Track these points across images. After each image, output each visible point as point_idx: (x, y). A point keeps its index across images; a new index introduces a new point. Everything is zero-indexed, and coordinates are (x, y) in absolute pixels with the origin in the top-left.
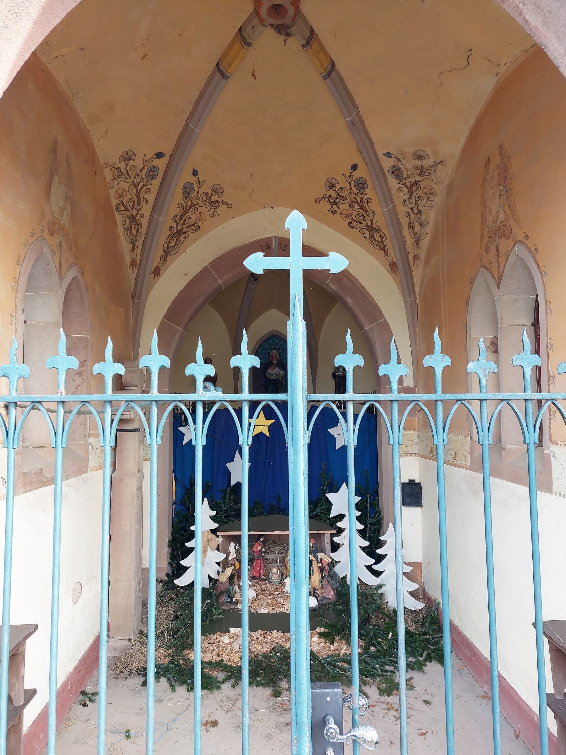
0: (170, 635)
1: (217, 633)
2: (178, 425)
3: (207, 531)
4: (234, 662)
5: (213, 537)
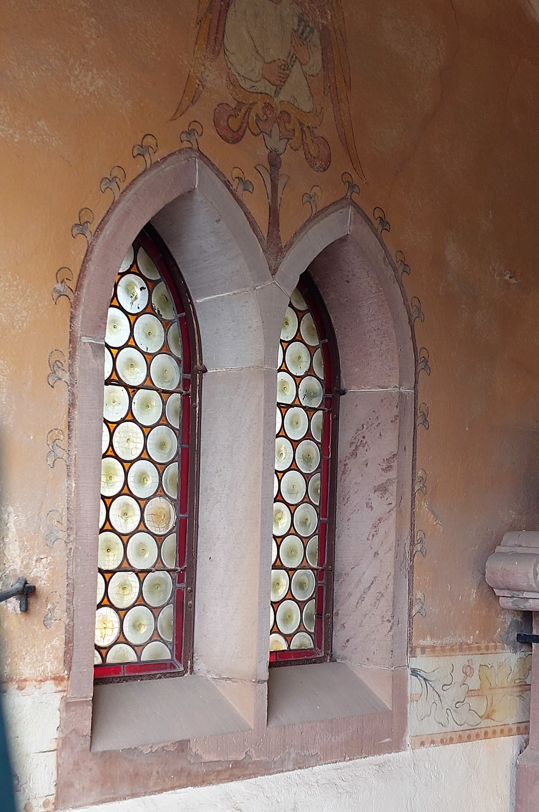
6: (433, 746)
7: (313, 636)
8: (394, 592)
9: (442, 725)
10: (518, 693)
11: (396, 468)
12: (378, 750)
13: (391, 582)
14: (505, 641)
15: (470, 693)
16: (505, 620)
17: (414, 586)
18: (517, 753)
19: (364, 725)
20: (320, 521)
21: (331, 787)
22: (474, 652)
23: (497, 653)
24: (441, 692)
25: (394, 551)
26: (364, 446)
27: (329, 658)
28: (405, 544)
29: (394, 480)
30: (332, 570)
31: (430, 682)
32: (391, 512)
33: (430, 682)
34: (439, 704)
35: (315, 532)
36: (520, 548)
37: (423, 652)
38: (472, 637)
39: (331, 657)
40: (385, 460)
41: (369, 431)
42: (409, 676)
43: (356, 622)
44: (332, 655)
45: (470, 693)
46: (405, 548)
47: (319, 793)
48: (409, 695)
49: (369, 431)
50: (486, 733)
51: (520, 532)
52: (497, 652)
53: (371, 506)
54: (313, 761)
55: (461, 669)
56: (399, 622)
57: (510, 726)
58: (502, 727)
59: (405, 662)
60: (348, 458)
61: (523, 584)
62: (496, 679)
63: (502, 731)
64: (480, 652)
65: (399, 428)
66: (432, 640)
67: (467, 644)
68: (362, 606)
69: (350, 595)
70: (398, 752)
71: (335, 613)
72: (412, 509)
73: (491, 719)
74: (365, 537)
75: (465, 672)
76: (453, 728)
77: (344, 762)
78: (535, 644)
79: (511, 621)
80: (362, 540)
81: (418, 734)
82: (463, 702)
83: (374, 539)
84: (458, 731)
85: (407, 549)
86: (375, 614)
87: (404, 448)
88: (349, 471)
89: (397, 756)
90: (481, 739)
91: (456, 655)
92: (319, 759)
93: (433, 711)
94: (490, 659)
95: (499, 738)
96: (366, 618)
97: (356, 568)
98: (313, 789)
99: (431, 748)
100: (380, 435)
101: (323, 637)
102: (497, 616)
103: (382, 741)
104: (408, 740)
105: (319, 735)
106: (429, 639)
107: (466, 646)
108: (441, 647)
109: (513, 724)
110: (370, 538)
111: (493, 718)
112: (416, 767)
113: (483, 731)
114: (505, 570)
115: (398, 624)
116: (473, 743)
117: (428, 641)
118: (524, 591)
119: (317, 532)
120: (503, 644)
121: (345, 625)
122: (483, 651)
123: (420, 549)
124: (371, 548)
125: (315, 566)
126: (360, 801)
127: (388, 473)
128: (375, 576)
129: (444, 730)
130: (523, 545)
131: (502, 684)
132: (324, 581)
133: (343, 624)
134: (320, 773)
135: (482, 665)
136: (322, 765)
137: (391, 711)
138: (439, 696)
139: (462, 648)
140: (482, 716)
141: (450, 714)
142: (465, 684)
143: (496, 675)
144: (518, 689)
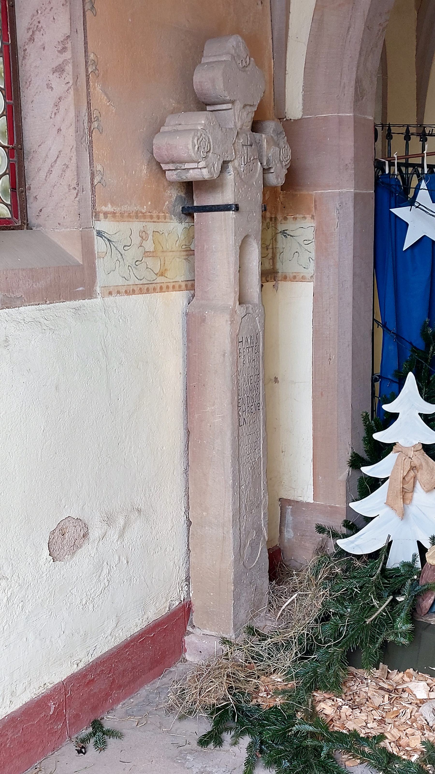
0: (303, 651)
1: (408, 671)
2: (393, 202)
3: (414, 447)
4: (407, 748)
5: (427, 463)
6: (119, 295)
7: (10, 207)
8: (77, 163)
9: (125, 279)
10: (185, 257)
11: (70, 48)
12: (73, 296)
13: (74, 154)
14: (173, 213)
15: (146, 254)
16: (172, 195)
17: (94, 159)
18: (186, 305)
19: (60, 275)
20: (7, 103)
21: (36, 324)
22: (147, 220)
23: (166, 222)
24: (123, 252)
25: (74, 126)
26: (40, 31)
27: (25, 226)
28: (84, 120)
29: (69, 61)
30: (22, 149)
31: (113, 243)
32: (69, 90)
33: (113, 243)
34: (122, 262)
35: (3, 113)
36: (180, 126)
37: (106, 217)
38: (145, 207)
39: (28, 225)
40: (60, 42)
41: (43, 16)
42: (95, 237)
43: (47, 193)
44: (28, 224)
45: (146, 254)
46: (84, 124)
47: (26, 329)
48: (96, 252)
49: (43, 16)
50: (161, 288)
51: (179, 114)
52: (166, 221)
53: (51, 87)
54: (19, 302)
55: (138, 233)
56: (83, 189)
57: (179, 283)
58: (174, 284)
59: (91, 225)
60: (26, 44)
61: (184, 155)
62: (167, 244)
63: (174, 287)
64: (152, 220)
65: (70, 11)
66: (112, 207)
67: (141, 212)
68: (50, 178)
69: (39, 170)
70: (91, 299)
71: (28, 188)
72: (88, 89)
73: (165, 276)
74: (48, 117)
75: (141, 236)
76: (135, 282)
77: (46, 305)
78: (196, 213)
79: (176, 195)
80: (46, 119)
81: (107, 286)
82: (141, 261)
83: (56, 117)
84: (139, 284)
85: (86, 125)
86: (63, 184)
87: (76, 31)
88: (28, 56)
89: (90, 302)
90: (157, 292)
91: (133, 221)
92: (24, 301)
93: (117, 267)
94: (160, 227)
95: (172, 292)
96: (55, 188)
97: (42, 146)
98: (21, 325)
99: (118, 297)
100: (54, 19)
101: (19, 208)
102: (165, 191)
103: (76, 289)
104: (98, 290)
105: (21, 281)
106: (109, 206)
107: (140, 214)
108: (121, 213)
109: (182, 281)
110: (53, 116)
111: (166, 276)
112: (107, 312)
113: (159, 286)
114: (169, 144)
115: (83, 191)
116: (151, 295)
117: (109, 208)
118: (185, 163)
119: (7, 172)
120: (171, 215)
121: (37, 197)
122: (155, 220)
123: (97, 126)
124: (54, 126)
125: (6, 145)
126: (61, 337)
127: (63, 54)
128: (59, 150)
129: (127, 283)
130: (183, 124)
131: (172, 249)
132: (15, 159)
133: (36, 196)
134: (25, 313)
135: (155, 232)
136: (26, 306)
137: (82, 265)
138: (121, 255)
139: (138, 216)
140: (157, 274)
141: (131, 270)
142: (142, 246)
143: (167, 240)
144: (185, 253)
